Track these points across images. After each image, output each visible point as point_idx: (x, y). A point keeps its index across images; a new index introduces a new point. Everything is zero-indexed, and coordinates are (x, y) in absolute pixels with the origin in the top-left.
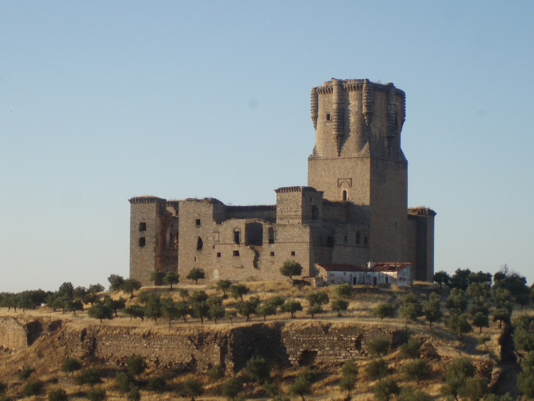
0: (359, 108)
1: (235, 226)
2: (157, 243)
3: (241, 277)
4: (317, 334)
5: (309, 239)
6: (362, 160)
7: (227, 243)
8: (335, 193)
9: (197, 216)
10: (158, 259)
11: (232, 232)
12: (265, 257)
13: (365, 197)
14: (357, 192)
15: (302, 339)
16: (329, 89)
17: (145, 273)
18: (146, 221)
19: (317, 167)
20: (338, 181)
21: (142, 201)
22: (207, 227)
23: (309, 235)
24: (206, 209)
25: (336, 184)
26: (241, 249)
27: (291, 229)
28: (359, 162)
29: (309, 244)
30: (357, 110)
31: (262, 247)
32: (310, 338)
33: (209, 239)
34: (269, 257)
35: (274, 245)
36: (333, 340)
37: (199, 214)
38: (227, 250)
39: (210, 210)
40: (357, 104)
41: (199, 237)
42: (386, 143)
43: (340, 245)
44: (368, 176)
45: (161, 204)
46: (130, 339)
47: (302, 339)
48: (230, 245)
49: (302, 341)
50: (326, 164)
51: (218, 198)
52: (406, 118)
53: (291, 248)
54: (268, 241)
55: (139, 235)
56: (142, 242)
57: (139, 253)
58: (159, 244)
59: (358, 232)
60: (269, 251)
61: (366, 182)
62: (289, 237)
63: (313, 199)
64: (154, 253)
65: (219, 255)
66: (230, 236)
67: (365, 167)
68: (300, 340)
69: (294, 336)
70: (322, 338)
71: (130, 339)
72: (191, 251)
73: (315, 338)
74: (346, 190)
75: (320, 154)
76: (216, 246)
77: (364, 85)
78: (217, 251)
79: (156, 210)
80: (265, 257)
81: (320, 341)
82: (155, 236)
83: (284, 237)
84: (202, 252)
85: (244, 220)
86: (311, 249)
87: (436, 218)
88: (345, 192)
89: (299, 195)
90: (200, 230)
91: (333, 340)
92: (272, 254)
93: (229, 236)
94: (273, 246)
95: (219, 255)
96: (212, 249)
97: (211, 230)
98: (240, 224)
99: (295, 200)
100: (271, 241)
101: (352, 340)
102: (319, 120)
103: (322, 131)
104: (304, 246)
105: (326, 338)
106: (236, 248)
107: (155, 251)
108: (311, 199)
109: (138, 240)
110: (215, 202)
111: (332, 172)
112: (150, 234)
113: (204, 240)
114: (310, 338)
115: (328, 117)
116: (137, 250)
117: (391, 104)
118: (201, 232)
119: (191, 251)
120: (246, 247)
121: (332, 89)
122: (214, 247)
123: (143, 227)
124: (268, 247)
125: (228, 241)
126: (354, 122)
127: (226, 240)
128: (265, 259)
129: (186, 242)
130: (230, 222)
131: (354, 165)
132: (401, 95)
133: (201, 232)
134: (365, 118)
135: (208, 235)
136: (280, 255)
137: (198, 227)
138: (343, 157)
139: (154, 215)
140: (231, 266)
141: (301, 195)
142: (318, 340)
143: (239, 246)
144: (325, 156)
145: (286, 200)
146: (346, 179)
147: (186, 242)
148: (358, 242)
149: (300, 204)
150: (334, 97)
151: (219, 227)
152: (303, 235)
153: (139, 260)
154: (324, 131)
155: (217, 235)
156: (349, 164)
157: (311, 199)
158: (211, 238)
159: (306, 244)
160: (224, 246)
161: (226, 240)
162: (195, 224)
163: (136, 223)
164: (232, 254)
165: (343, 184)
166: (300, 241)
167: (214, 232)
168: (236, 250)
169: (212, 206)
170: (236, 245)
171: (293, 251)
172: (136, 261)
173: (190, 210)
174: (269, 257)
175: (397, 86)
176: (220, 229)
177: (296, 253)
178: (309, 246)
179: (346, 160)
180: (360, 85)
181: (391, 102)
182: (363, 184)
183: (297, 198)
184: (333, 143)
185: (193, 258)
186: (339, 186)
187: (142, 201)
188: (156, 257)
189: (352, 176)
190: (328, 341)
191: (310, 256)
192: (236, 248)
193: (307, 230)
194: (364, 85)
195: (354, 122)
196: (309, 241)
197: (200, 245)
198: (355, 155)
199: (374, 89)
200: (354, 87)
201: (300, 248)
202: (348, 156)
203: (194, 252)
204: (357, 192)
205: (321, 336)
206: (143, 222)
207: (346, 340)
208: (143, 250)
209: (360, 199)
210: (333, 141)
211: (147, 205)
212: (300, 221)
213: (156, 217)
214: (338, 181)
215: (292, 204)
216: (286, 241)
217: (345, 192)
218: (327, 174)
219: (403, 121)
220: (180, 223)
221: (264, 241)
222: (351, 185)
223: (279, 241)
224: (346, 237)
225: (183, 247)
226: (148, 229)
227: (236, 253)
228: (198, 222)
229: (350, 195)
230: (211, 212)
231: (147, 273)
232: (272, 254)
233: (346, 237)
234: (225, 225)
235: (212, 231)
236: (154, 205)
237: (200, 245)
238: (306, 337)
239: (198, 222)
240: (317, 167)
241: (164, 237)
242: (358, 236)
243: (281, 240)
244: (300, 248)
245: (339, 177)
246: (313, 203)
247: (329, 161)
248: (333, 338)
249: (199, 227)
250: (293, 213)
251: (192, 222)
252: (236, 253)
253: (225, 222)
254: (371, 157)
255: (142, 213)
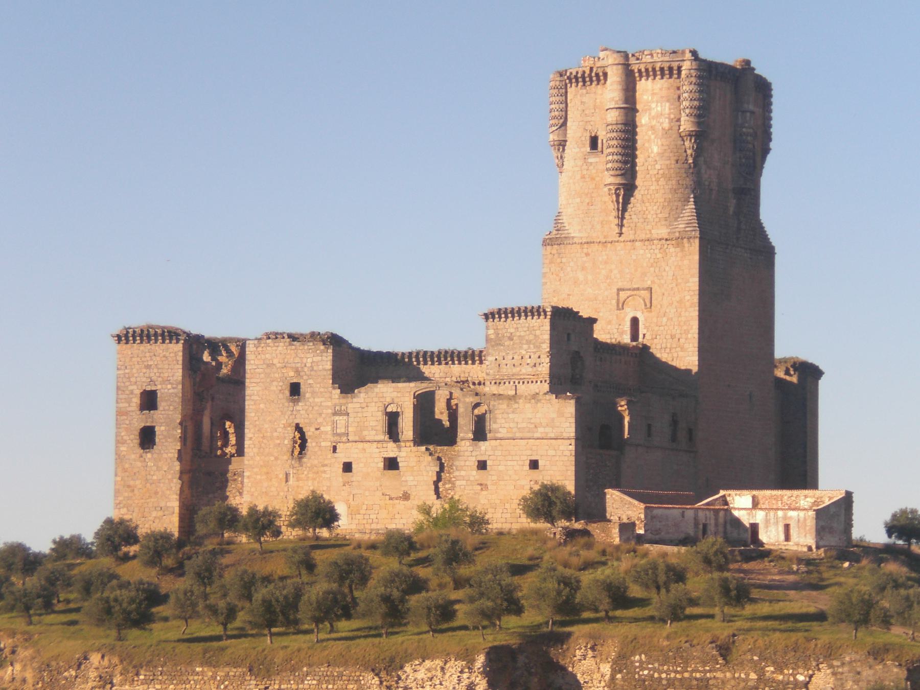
0: (671, 120)
1: (388, 400)
2: (183, 439)
3: (404, 521)
4: (704, 663)
5: (574, 430)
6: (678, 245)
7: (367, 438)
8: (609, 323)
9: (292, 374)
10: (186, 477)
11: (380, 414)
12: (463, 473)
13: (687, 332)
14: (665, 319)
15: (664, 676)
16: (597, 75)
17: (154, 514)
18: (159, 387)
19: (564, 260)
20: (618, 294)
21: (148, 336)
22: (317, 400)
23: (573, 420)
24: (315, 359)
25: (614, 302)
26: (403, 454)
27: (528, 406)
28: (672, 250)
29: (573, 442)
30: (666, 125)
31: (456, 448)
32: (686, 675)
33: (322, 429)
34: (474, 473)
35: (487, 443)
36: (746, 680)
37: (297, 371)
38: (369, 456)
39: (324, 360)
40: (667, 111)
41: (297, 425)
42: (732, 204)
43: (638, 445)
44: (693, 283)
45: (195, 345)
46: (214, 678)
47: (664, 676)
48: (375, 444)
49: (664, 682)
50: (587, 254)
51: (341, 333)
52: (772, 145)
53: (529, 452)
54: (471, 436)
55: (139, 420)
56: (147, 438)
57: (139, 464)
58: (189, 443)
59: (674, 415)
60: (474, 459)
61: (688, 298)
62: (524, 425)
63: (573, 337)
64: (177, 463)
65: (347, 467)
66: (378, 422)
67: (686, 262)
68: (660, 679)
69: (643, 669)
70: (719, 675)
71: (214, 678)
72: (276, 459)
73: (698, 675)
74: (639, 315)
75: (574, 229)
76: (340, 447)
77: (686, 66)
78: (343, 456)
79: (183, 360)
80: (463, 473)
81: (711, 682)
82: (181, 424)
83: (512, 425)
84: (304, 460)
85: (412, 384)
86: (576, 456)
87: (822, 383)
88: (635, 322)
89: (542, 328)
90: (298, 408)
91: (746, 680)
92: (482, 465)
93: (373, 424)
94: (483, 445)
95: (347, 467)
96: (330, 454)
97: (328, 407)
98: (400, 396)
99: (531, 337)
100: (480, 434)
101: (795, 680)
102: (571, 150)
103: (578, 176)
104: (562, 448)
105: (728, 675)
106: (391, 450)
107: (180, 458)
108: (569, 335)
109: (137, 433)
110: (335, 342)
111: (603, 272)
112: (168, 420)
113: (309, 432)
114: (686, 675)
115: (594, 142)
116: (133, 456)
117: (744, 112)
118: (302, 413)
119: (276, 459)
120: (415, 449)
121: (605, 75)
122: (335, 449)
123: (149, 401)
124: (470, 449)
125: (370, 435)
126: (661, 155)
127: (365, 433)
128: (463, 478)
129: (263, 437)
130: (376, 390)
131: (659, 256)
132: (763, 88)
133: (302, 413)
134: (687, 143)
135: (320, 420)
136: (501, 468)
137: (295, 402)
138: (632, 237)
139: (178, 373)
140: (379, 493)
141: (547, 327)
142: (708, 680)
143: (399, 447)
144: (584, 234)
145: (511, 339)
146: (638, 289)
147: (263, 437)
148: (674, 439)
149: (546, 347)
150: (610, 93)
151: (349, 400)
152: (560, 418)
153: (138, 482)
154: (583, 177)
155: (342, 420)
156: (644, 253)
157: (569, 335)
158: (329, 428)
159: (569, 442)
160: (360, 445)
161: (365, 433)
162: (287, 393)
163: (132, 392)
164: (381, 465)
165: (630, 301)
166: (553, 435)
167: (335, 414)
168: (392, 455)
169: (330, 351)
170: (391, 445)
171: (534, 458)
172: (132, 483)
173: (275, 361)
174: (475, 474)
175: (761, 69)
176: (350, 405)
177: (540, 463)
178: (573, 448)
179: (638, 244)
180: (675, 65)
181: (746, 106)
182: (680, 302)
183: (538, 333)
184: (607, 202)
185: (282, 476)
186: (621, 306)
187: (148, 336)
188: (181, 472)
189: (653, 282)
190: (733, 683)
191: (576, 471)
192: (391, 450)
193: (569, 408)
194: (686, 66)
195: (658, 154)
196: (573, 434)
197: (302, 442)
198: (663, 232)
199: (712, 75)
200: (662, 69)
201: (551, 452)
202: (643, 236)
203: (283, 462)
204: (665, 319)
205: (716, 670)
206: (149, 388)
207: (782, 682)
208: (149, 455)
209: (673, 337)
210: (607, 198)
211: (159, 348)
212: (546, 387)
213: (183, 376)
214: (618, 294)
215: (525, 346)
216: (518, 435)
217: (635, 322)
218: (590, 277)
219: (766, 151)
220: (248, 392)
221: (461, 435)
222: (649, 306)
223: (499, 435)
224: (649, 426)
225: (255, 450)
226: (162, 405)
227: (392, 464)
228: (295, 389)
229: (645, 327)
230: (329, 366)
231: (160, 513)
232: (482, 465)
233: (649, 426)
234: (362, 395)
235: (330, 411)
236: (176, 350)
237: (302, 442)
238: (676, 672)
239: (295, 389)
240: (564, 260)
241: (198, 426)
242: (674, 423)
243: (503, 433)
244: (551, 452)
245: (620, 285)
246: (575, 348)
247: (595, 247)
248: (747, 675)
249: (298, 401)
250: (526, 370)
251: (279, 390)
252: (392, 464)
253: (363, 389)
254: (701, 239)
255: (148, 367)
